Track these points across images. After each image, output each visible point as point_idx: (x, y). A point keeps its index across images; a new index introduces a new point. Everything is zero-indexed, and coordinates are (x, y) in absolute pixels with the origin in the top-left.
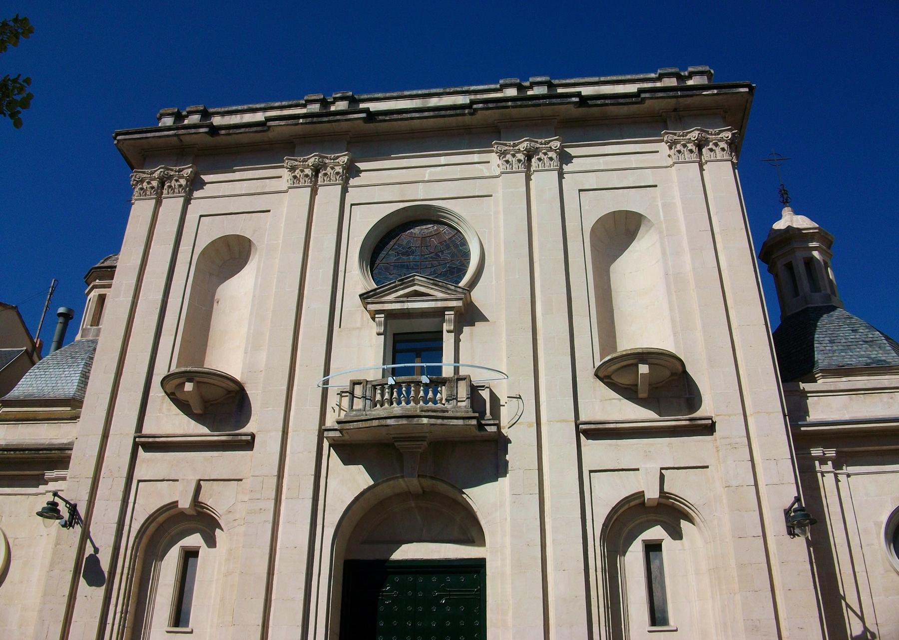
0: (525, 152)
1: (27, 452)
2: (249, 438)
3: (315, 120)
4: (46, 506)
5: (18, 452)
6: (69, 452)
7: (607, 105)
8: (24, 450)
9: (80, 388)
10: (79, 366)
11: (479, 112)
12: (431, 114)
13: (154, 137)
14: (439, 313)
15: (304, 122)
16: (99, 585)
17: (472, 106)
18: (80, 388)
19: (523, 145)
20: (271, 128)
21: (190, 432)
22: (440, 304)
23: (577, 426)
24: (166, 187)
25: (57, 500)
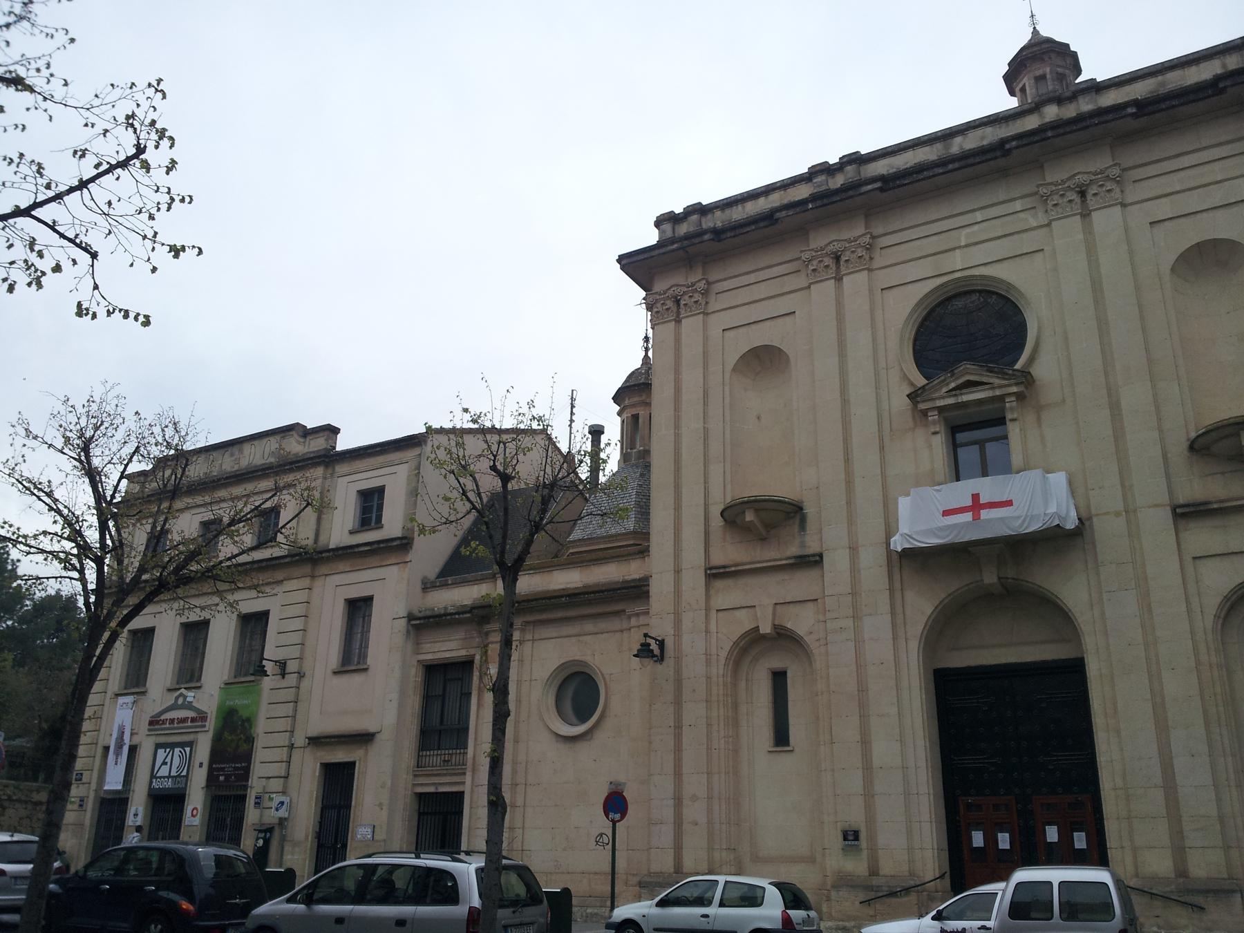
0: (1077, 189)
1: (606, 593)
2: (818, 558)
3: (825, 201)
4: (640, 647)
5: (597, 594)
6: (648, 588)
7: (1173, 107)
8: (602, 591)
9: (638, 519)
10: (632, 497)
11: (1014, 151)
12: (957, 165)
13: (659, 254)
14: (1001, 398)
15: (814, 206)
16: (126, 119)
17: (1004, 146)
18: (638, 519)
19: (1074, 181)
20: (779, 221)
21: (758, 559)
22: (998, 392)
23: (1174, 509)
24: (682, 306)
25: (649, 640)
